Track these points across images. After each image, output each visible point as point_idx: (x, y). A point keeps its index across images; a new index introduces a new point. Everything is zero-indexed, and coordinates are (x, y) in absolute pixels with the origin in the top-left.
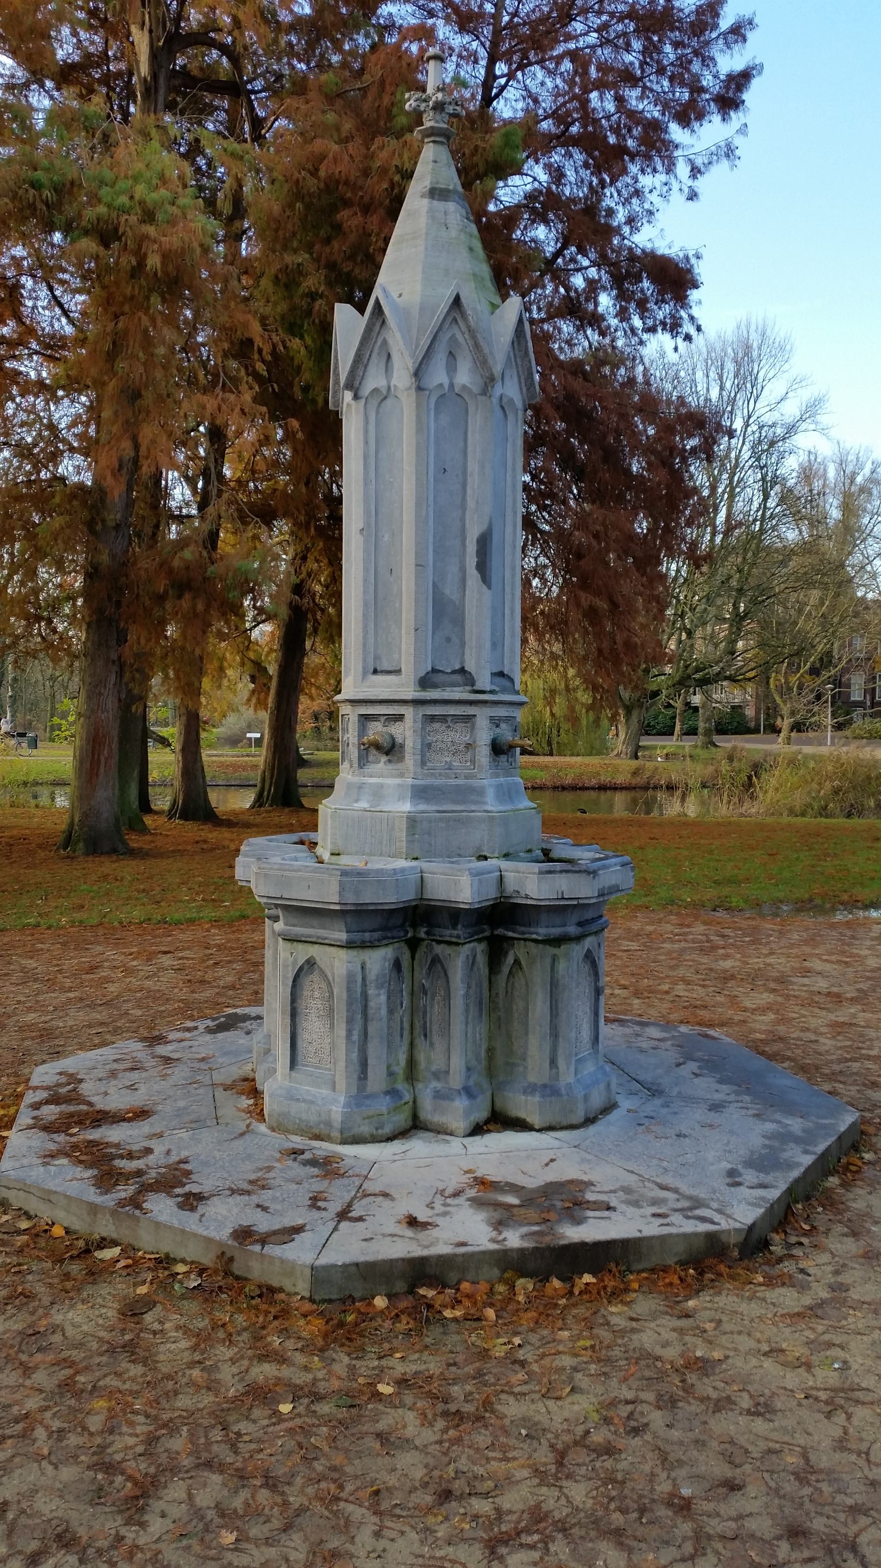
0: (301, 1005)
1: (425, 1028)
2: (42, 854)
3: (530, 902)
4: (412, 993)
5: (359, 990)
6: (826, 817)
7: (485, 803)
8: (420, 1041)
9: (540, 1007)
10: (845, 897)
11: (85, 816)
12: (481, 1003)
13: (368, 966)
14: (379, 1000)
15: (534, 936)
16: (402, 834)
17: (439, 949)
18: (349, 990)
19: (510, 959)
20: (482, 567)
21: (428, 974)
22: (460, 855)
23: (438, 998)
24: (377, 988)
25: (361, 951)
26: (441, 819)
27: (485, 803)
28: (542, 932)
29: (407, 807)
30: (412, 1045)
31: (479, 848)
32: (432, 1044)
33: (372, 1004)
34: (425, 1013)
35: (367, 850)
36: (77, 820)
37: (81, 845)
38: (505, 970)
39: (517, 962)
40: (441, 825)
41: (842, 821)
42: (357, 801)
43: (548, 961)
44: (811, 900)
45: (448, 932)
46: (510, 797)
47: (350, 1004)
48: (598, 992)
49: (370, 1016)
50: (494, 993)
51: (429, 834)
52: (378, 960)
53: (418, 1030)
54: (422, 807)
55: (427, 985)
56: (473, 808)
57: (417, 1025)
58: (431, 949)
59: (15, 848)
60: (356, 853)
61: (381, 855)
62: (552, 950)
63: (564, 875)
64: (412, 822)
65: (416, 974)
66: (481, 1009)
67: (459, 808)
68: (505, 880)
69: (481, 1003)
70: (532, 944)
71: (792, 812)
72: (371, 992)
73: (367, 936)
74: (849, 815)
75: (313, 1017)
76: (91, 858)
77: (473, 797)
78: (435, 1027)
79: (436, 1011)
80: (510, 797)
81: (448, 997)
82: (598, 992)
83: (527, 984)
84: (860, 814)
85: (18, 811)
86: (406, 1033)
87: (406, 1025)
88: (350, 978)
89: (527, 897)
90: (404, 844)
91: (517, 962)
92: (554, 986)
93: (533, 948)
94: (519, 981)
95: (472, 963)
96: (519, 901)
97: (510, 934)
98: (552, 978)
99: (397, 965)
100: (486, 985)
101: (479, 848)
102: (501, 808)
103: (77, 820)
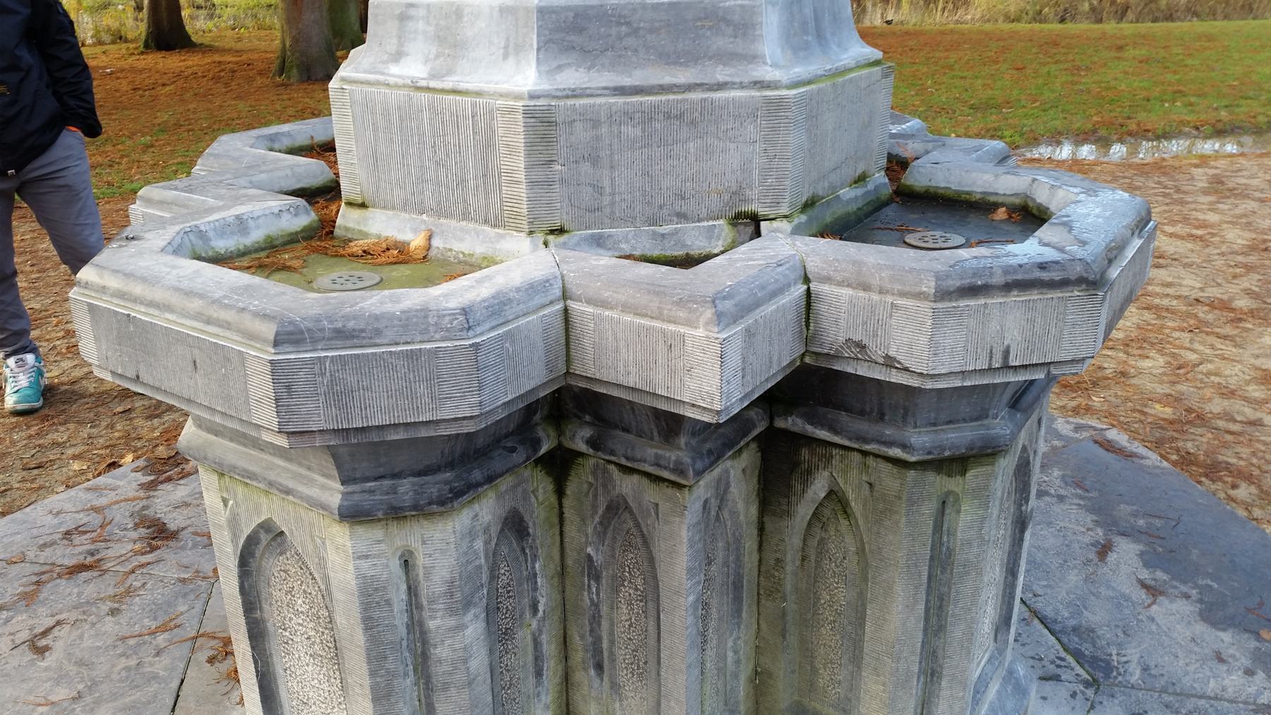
0: (272, 616)
1: (597, 650)
2: (259, 81)
3: (896, 378)
4: (563, 572)
5: (400, 620)
6: (1040, 22)
7: (754, 58)
8: (585, 678)
9: (897, 616)
10: (1133, 127)
11: (295, 41)
12: (737, 586)
13: (421, 561)
14: (461, 640)
15: (896, 452)
16: (514, 162)
17: (627, 486)
18: (369, 623)
19: (819, 488)
20: (688, 262)
21: (601, 535)
22: (682, 216)
23: (626, 591)
24: (451, 611)
25: (394, 528)
26: (628, 115)
27: (754, 58)
28: (921, 440)
29: (524, 77)
30: (567, 681)
31: (738, 194)
32: (615, 687)
33: (442, 651)
34: (596, 619)
35: (430, 202)
36: (288, 44)
37: (295, 71)
38: (804, 510)
39: (834, 495)
40: (630, 131)
41: (1056, 27)
42: (398, 56)
43: (928, 509)
44: (1094, 131)
45: (651, 452)
46: (820, 36)
47: (376, 658)
48: (1021, 524)
49: (437, 680)
50: (770, 558)
51: (595, 161)
52: (447, 545)
53: (579, 655)
54: (573, 77)
55: (598, 559)
56: (721, 74)
57: (576, 641)
58: (607, 483)
59: (238, 74)
60: (405, 207)
61: (465, 216)
62: (937, 483)
63: (1015, 297)
64: (543, 124)
65: (571, 530)
66: (738, 599)
67: (682, 76)
68: (820, 307)
69: (737, 586)
70: (886, 467)
71: (1009, 19)
72: (436, 623)
73: (406, 487)
74: (1062, 20)
75: (300, 649)
76: (305, 86)
77: (721, 42)
78: (622, 654)
79: (622, 617)
80: (820, 36)
81: (652, 596)
82: (1021, 524)
83: (861, 551)
84: (1073, 18)
85: (263, 33)
86: (552, 668)
87: (550, 648)
88: (371, 598)
89: (890, 363)
90: (522, 191)
91: (834, 495)
92: (941, 565)
93: (888, 477)
94: (842, 541)
95: (713, 515)
96: (863, 370)
97: (823, 434)
98: (937, 545)
99: (515, 526)
100: (750, 544)
101: (738, 194)
102: (800, 71)
103: (288, 44)
